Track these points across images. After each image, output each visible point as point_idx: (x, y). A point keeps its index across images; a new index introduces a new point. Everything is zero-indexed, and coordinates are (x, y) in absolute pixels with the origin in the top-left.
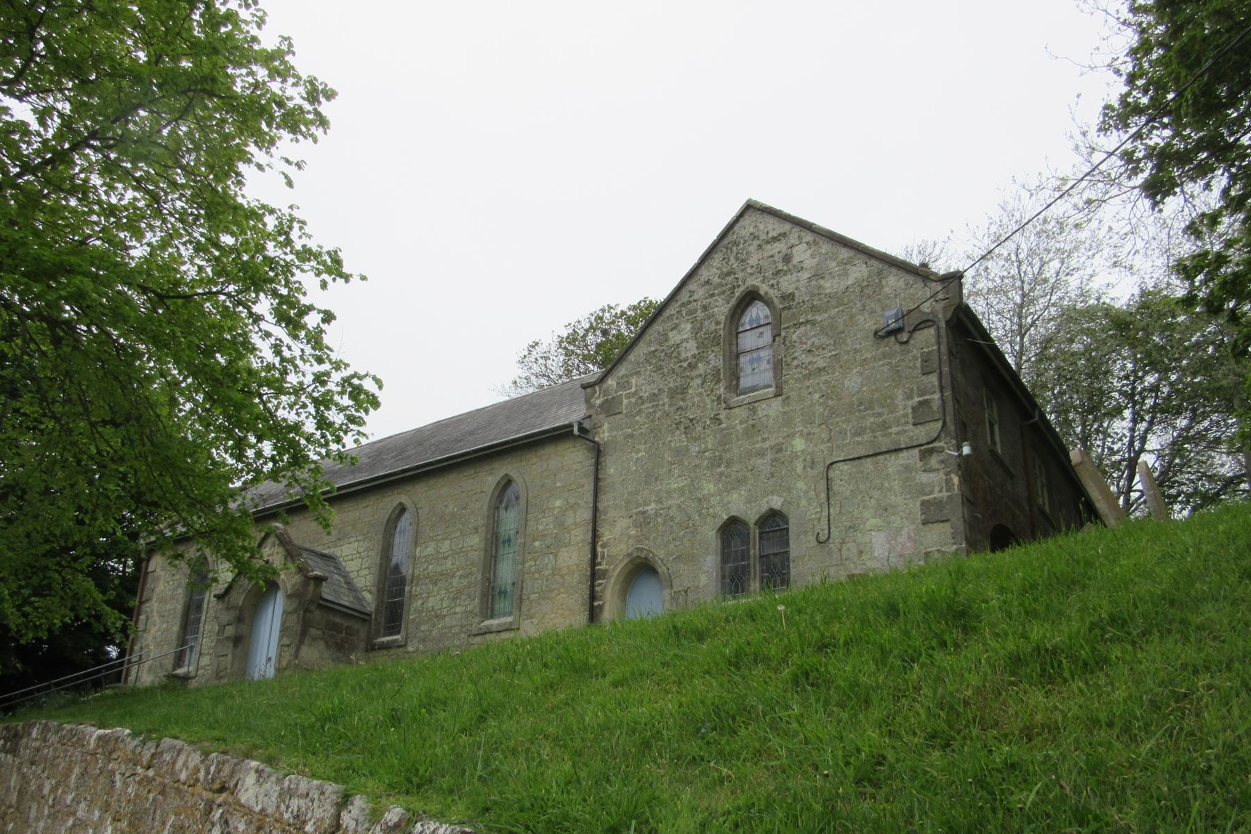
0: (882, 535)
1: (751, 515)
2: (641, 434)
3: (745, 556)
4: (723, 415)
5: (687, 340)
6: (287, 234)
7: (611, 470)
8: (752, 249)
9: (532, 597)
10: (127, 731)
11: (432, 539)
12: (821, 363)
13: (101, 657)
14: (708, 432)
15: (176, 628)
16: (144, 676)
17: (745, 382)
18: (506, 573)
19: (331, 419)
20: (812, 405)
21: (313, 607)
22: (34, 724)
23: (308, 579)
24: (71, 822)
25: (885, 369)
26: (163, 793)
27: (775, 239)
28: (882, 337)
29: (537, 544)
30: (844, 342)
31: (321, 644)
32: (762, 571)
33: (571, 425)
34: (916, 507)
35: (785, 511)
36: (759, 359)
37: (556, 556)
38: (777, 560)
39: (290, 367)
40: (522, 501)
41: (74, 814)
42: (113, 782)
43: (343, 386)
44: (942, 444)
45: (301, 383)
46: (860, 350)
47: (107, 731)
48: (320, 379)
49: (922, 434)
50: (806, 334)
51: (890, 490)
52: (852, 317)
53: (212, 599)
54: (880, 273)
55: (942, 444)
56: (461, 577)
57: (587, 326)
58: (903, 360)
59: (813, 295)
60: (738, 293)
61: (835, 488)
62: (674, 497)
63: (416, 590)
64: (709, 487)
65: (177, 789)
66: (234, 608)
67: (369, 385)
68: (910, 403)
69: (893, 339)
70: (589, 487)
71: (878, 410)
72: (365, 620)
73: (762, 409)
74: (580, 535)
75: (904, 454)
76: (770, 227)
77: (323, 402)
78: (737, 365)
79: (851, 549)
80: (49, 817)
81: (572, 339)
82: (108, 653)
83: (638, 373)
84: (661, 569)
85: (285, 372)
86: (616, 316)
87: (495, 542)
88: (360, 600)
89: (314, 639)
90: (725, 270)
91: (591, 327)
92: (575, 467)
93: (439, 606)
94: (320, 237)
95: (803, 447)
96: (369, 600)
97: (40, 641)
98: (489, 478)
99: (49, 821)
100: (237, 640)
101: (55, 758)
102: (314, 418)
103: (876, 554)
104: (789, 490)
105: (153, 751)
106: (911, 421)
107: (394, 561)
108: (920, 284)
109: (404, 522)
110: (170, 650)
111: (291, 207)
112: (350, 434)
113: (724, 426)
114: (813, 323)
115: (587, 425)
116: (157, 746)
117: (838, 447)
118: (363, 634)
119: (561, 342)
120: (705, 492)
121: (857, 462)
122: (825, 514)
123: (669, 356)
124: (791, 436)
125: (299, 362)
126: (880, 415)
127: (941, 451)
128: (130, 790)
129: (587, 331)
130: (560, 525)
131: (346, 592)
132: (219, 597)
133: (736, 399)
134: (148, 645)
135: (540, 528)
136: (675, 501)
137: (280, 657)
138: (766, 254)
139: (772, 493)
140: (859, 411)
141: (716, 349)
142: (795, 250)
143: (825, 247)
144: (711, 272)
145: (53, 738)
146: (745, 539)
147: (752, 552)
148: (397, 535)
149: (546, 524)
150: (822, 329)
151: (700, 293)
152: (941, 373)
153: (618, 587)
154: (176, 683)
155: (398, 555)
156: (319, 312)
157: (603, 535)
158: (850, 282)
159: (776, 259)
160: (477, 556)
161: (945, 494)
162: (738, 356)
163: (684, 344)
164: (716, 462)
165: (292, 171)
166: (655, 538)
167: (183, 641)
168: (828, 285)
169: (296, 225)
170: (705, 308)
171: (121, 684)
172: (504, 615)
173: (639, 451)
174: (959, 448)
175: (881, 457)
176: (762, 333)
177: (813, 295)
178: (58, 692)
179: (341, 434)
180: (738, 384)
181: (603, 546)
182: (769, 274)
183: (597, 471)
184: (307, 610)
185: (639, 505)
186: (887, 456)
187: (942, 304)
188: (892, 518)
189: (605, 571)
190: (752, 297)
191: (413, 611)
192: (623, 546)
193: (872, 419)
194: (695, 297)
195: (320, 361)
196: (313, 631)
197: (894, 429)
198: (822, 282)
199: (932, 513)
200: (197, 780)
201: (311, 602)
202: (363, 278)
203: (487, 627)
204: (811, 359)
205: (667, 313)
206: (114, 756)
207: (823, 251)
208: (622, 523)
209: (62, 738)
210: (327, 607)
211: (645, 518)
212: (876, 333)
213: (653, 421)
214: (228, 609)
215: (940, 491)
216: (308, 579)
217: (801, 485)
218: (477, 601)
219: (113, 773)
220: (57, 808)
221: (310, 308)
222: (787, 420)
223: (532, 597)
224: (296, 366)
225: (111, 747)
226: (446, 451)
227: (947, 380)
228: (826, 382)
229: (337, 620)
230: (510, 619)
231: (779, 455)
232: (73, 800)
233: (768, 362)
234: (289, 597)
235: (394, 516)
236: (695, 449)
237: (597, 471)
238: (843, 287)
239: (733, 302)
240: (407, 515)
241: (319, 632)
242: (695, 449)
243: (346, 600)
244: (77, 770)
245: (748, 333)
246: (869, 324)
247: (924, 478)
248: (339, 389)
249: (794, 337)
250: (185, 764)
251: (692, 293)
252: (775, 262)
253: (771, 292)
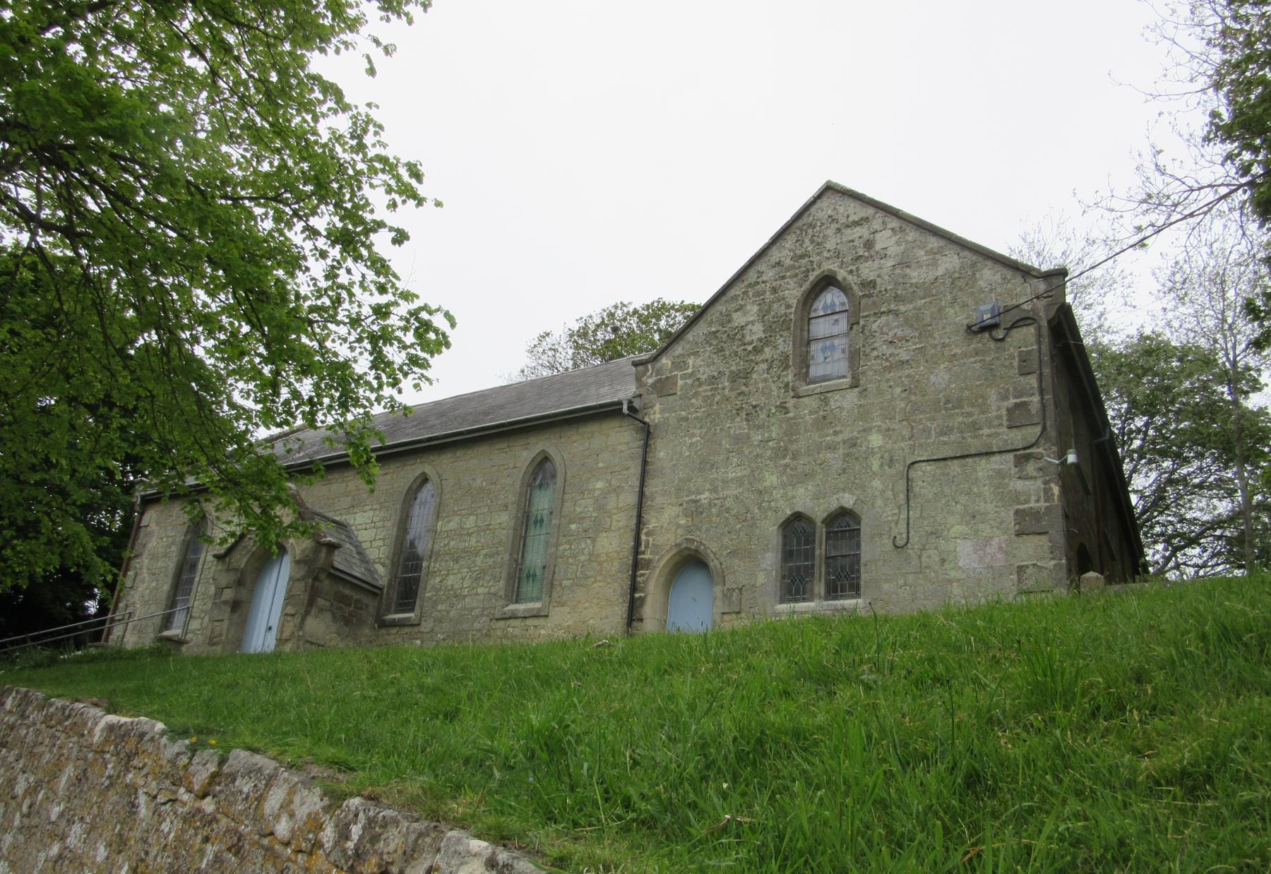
0: (969, 543)
1: (819, 512)
2: (697, 418)
3: (809, 555)
4: (791, 403)
5: (753, 323)
6: (360, 138)
7: (662, 452)
8: (830, 232)
9: (565, 583)
10: (160, 726)
11: (455, 513)
12: (904, 356)
13: (78, 612)
14: (773, 420)
15: (166, 588)
16: (130, 633)
17: (814, 371)
18: (535, 558)
19: (391, 358)
20: (893, 399)
21: (323, 576)
22: (10, 691)
23: (319, 544)
24: (55, 849)
25: (977, 366)
26: (236, 849)
27: (856, 224)
28: (975, 333)
29: (573, 527)
30: (931, 335)
31: (328, 616)
32: (828, 573)
33: (620, 403)
34: (1009, 516)
35: (857, 510)
36: (832, 348)
37: (594, 540)
38: (847, 561)
39: (344, 294)
40: (560, 480)
41: (63, 838)
42: (133, 805)
43: (408, 321)
44: (1040, 450)
45: (358, 314)
46: (949, 345)
47: (124, 720)
48: (381, 312)
49: (1018, 438)
50: (887, 324)
51: (979, 495)
52: (941, 309)
53: (210, 558)
54: (973, 265)
55: (1040, 450)
56: (486, 555)
57: (599, 321)
58: (998, 359)
59: (897, 284)
60: (812, 277)
61: (917, 489)
62: (731, 485)
63: (435, 566)
64: (771, 479)
65: (268, 849)
66: (235, 570)
67: (439, 321)
68: (1005, 404)
69: (987, 335)
70: (635, 469)
71: (967, 409)
72: (375, 594)
73: (835, 401)
74: (622, 521)
75: (997, 458)
76: (851, 210)
77: (379, 339)
78: (808, 352)
79: (931, 557)
80: (20, 829)
81: (583, 333)
82: (87, 608)
83: (696, 354)
84: (713, 564)
85: (338, 301)
86: (628, 313)
87: (526, 521)
88: (372, 572)
89: (321, 610)
90: (798, 252)
91: (603, 322)
92: (621, 448)
93: (461, 585)
94: (397, 143)
95: (881, 443)
96: (382, 574)
97: (16, 588)
98: (524, 453)
99: (21, 838)
100: (236, 605)
101: (35, 744)
102: (371, 354)
103: (961, 564)
104: (863, 487)
105: (213, 768)
106: (1005, 423)
107: (410, 537)
108: (1019, 280)
109: (426, 493)
110: (158, 611)
111: (369, 105)
112: (411, 376)
113: (791, 415)
114: (897, 314)
115: (637, 404)
116: (222, 761)
117: (921, 445)
119: (571, 336)
120: (767, 484)
121: (942, 463)
122: (903, 516)
123: (731, 338)
124: (867, 431)
125: (356, 290)
126: (970, 414)
127: (1038, 458)
128: (165, 827)
129: (598, 326)
130: (601, 508)
132: (219, 557)
133: (804, 388)
134: (134, 603)
135: (578, 510)
136: (732, 491)
137: (281, 630)
138: (845, 239)
139: (844, 490)
140: (946, 409)
141: (785, 334)
142: (878, 236)
143: (912, 235)
144: (782, 254)
145: (34, 716)
146: (809, 539)
147: (817, 552)
148: (417, 507)
149: (585, 506)
150: (906, 319)
151: (769, 274)
152: (1041, 374)
153: (662, 579)
154: (167, 648)
155: (418, 525)
156: (391, 229)
157: (648, 522)
158: (940, 273)
159: (856, 243)
160: (505, 534)
161: (1043, 504)
162: (809, 342)
163: (749, 327)
164: (781, 452)
165: (377, 54)
166: (707, 530)
167: (172, 603)
168: (914, 274)
169: (371, 128)
170: (774, 290)
171: (102, 642)
172: (532, 600)
173: (693, 435)
174: (1062, 454)
175: (970, 460)
176: (837, 321)
177: (897, 284)
178: (35, 647)
179: (400, 376)
180: (807, 372)
181: (648, 534)
182: (848, 259)
183: (645, 452)
184: (316, 579)
185: (690, 493)
186: (977, 459)
187: (1044, 302)
188: (981, 526)
189: (649, 562)
190: (828, 281)
191: (429, 588)
192: (671, 536)
193: (960, 419)
194: (764, 278)
195: (382, 289)
196: (320, 602)
197: (986, 431)
198: (908, 271)
199: (1027, 524)
200: (318, 844)
201: (322, 570)
202: (438, 204)
203: (513, 611)
204: (892, 350)
205: (732, 293)
206: (135, 762)
207: (910, 238)
208: (670, 512)
209: (49, 717)
210: (338, 577)
211: (697, 508)
212: (969, 327)
213: (711, 405)
214: (228, 570)
215: (1037, 501)
216: (319, 544)
217: (877, 484)
218: (502, 584)
219: (132, 790)
220: (35, 821)
221: (380, 225)
222: (863, 413)
223: (565, 583)
224: (351, 295)
225: (131, 745)
226: (475, 422)
227: (1048, 382)
228: (909, 376)
229: (347, 592)
230: (538, 605)
231: (853, 450)
232: (61, 815)
233: (843, 351)
234: (298, 562)
235: (415, 487)
236: (756, 437)
237: (645, 452)
238: (931, 277)
239: (807, 285)
240: (429, 486)
241: (327, 604)
242: (756, 437)
244: (69, 771)
245: (821, 320)
246: (959, 317)
247: (1019, 485)
248: (402, 324)
249: (874, 327)
250: (286, 806)
251: (761, 273)
252: (855, 247)
253: (850, 278)
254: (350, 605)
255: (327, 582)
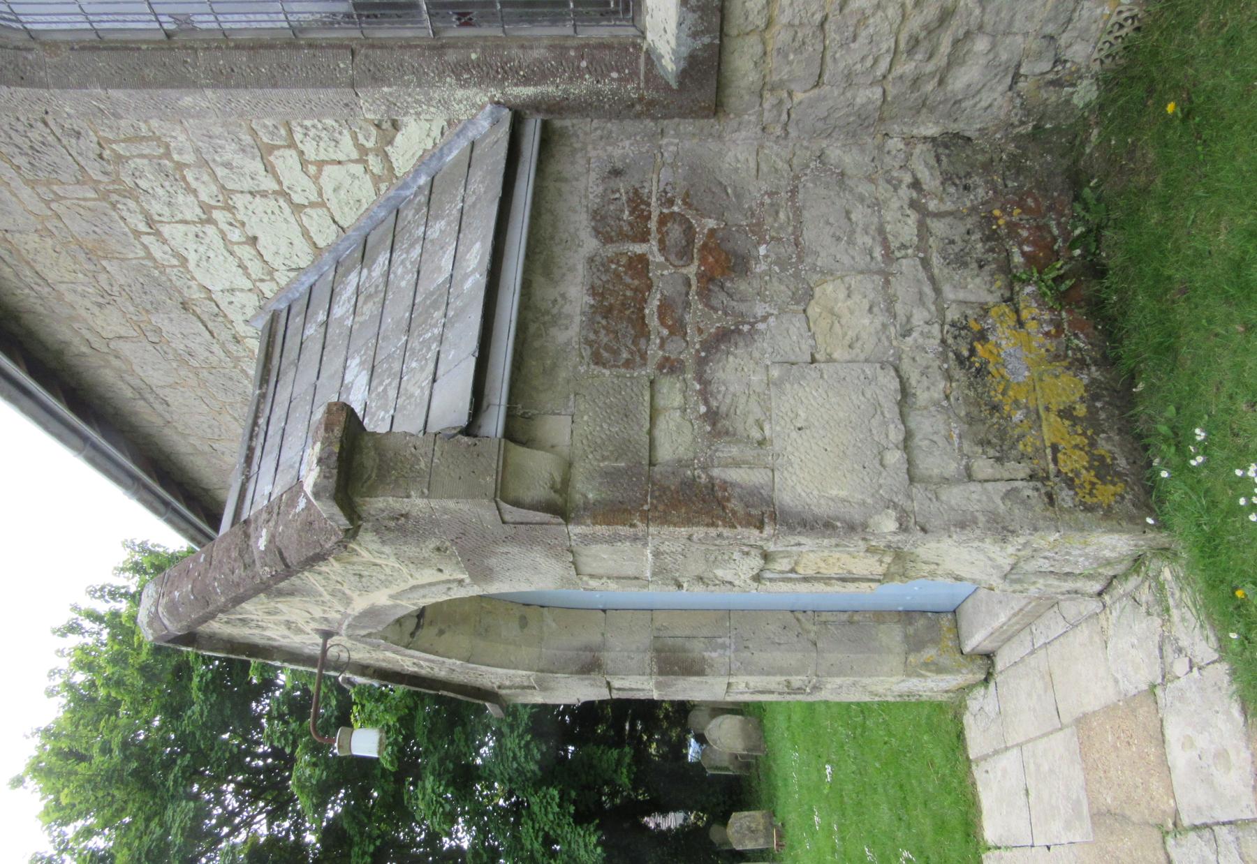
21: (538, 469)
31: (737, 374)
88: (434, 187)
118: (625, 143)
131: (408, 256)
196: (675, 440)
229: (573, 294)
241: (672, 394)
243: (457, 258)
254: (639, 265)
255: (558, 429)
